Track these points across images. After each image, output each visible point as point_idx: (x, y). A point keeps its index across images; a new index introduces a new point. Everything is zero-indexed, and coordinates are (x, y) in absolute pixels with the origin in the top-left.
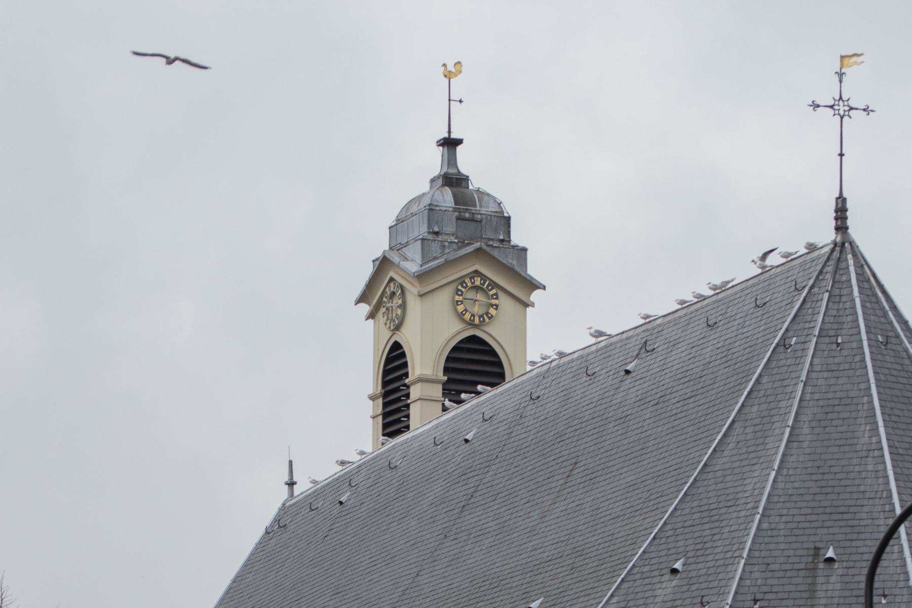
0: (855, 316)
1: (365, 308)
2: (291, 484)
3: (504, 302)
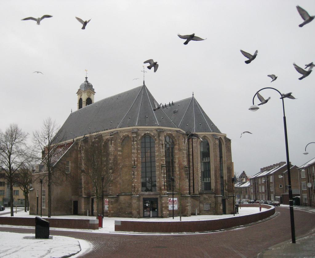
0: (36, 213)
1: (77, 94)
2: (72, 111)
3: (92, 94)
